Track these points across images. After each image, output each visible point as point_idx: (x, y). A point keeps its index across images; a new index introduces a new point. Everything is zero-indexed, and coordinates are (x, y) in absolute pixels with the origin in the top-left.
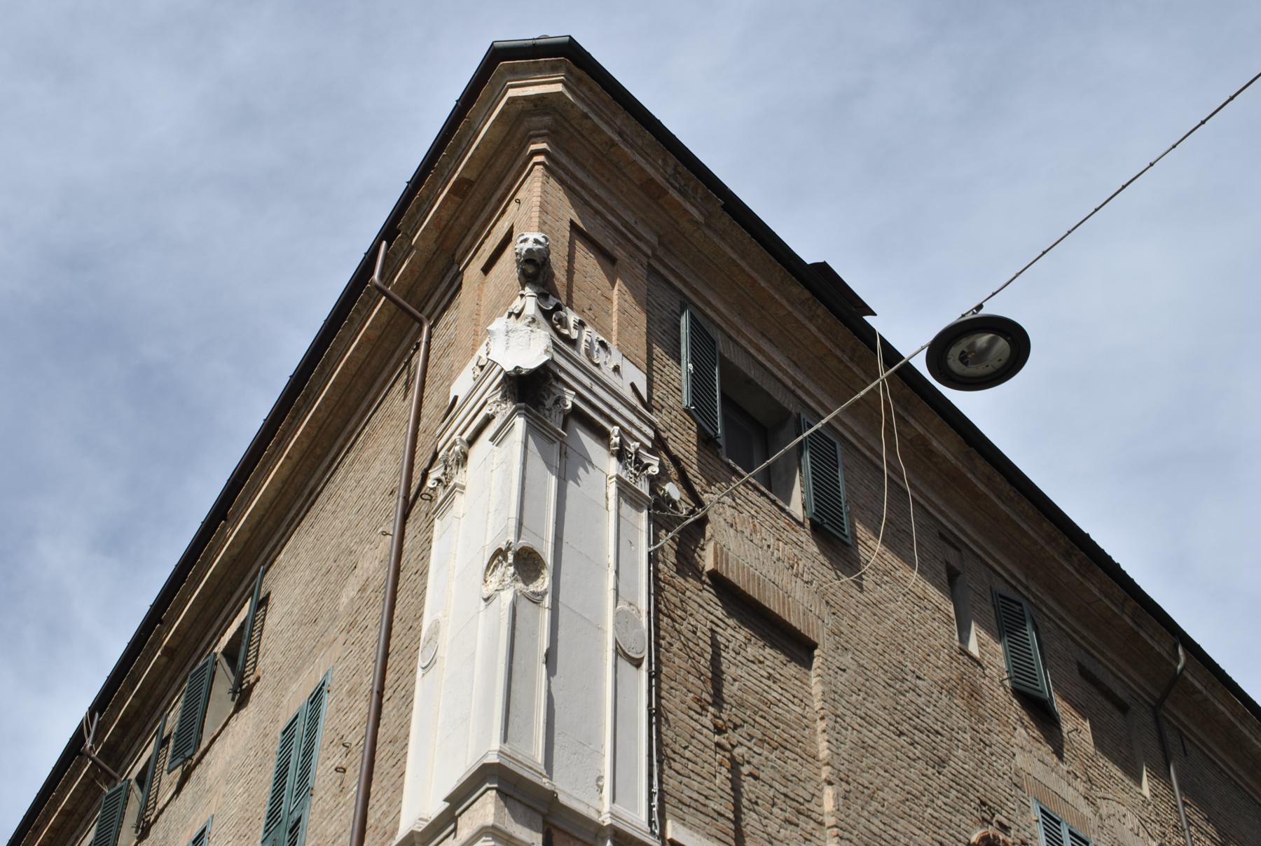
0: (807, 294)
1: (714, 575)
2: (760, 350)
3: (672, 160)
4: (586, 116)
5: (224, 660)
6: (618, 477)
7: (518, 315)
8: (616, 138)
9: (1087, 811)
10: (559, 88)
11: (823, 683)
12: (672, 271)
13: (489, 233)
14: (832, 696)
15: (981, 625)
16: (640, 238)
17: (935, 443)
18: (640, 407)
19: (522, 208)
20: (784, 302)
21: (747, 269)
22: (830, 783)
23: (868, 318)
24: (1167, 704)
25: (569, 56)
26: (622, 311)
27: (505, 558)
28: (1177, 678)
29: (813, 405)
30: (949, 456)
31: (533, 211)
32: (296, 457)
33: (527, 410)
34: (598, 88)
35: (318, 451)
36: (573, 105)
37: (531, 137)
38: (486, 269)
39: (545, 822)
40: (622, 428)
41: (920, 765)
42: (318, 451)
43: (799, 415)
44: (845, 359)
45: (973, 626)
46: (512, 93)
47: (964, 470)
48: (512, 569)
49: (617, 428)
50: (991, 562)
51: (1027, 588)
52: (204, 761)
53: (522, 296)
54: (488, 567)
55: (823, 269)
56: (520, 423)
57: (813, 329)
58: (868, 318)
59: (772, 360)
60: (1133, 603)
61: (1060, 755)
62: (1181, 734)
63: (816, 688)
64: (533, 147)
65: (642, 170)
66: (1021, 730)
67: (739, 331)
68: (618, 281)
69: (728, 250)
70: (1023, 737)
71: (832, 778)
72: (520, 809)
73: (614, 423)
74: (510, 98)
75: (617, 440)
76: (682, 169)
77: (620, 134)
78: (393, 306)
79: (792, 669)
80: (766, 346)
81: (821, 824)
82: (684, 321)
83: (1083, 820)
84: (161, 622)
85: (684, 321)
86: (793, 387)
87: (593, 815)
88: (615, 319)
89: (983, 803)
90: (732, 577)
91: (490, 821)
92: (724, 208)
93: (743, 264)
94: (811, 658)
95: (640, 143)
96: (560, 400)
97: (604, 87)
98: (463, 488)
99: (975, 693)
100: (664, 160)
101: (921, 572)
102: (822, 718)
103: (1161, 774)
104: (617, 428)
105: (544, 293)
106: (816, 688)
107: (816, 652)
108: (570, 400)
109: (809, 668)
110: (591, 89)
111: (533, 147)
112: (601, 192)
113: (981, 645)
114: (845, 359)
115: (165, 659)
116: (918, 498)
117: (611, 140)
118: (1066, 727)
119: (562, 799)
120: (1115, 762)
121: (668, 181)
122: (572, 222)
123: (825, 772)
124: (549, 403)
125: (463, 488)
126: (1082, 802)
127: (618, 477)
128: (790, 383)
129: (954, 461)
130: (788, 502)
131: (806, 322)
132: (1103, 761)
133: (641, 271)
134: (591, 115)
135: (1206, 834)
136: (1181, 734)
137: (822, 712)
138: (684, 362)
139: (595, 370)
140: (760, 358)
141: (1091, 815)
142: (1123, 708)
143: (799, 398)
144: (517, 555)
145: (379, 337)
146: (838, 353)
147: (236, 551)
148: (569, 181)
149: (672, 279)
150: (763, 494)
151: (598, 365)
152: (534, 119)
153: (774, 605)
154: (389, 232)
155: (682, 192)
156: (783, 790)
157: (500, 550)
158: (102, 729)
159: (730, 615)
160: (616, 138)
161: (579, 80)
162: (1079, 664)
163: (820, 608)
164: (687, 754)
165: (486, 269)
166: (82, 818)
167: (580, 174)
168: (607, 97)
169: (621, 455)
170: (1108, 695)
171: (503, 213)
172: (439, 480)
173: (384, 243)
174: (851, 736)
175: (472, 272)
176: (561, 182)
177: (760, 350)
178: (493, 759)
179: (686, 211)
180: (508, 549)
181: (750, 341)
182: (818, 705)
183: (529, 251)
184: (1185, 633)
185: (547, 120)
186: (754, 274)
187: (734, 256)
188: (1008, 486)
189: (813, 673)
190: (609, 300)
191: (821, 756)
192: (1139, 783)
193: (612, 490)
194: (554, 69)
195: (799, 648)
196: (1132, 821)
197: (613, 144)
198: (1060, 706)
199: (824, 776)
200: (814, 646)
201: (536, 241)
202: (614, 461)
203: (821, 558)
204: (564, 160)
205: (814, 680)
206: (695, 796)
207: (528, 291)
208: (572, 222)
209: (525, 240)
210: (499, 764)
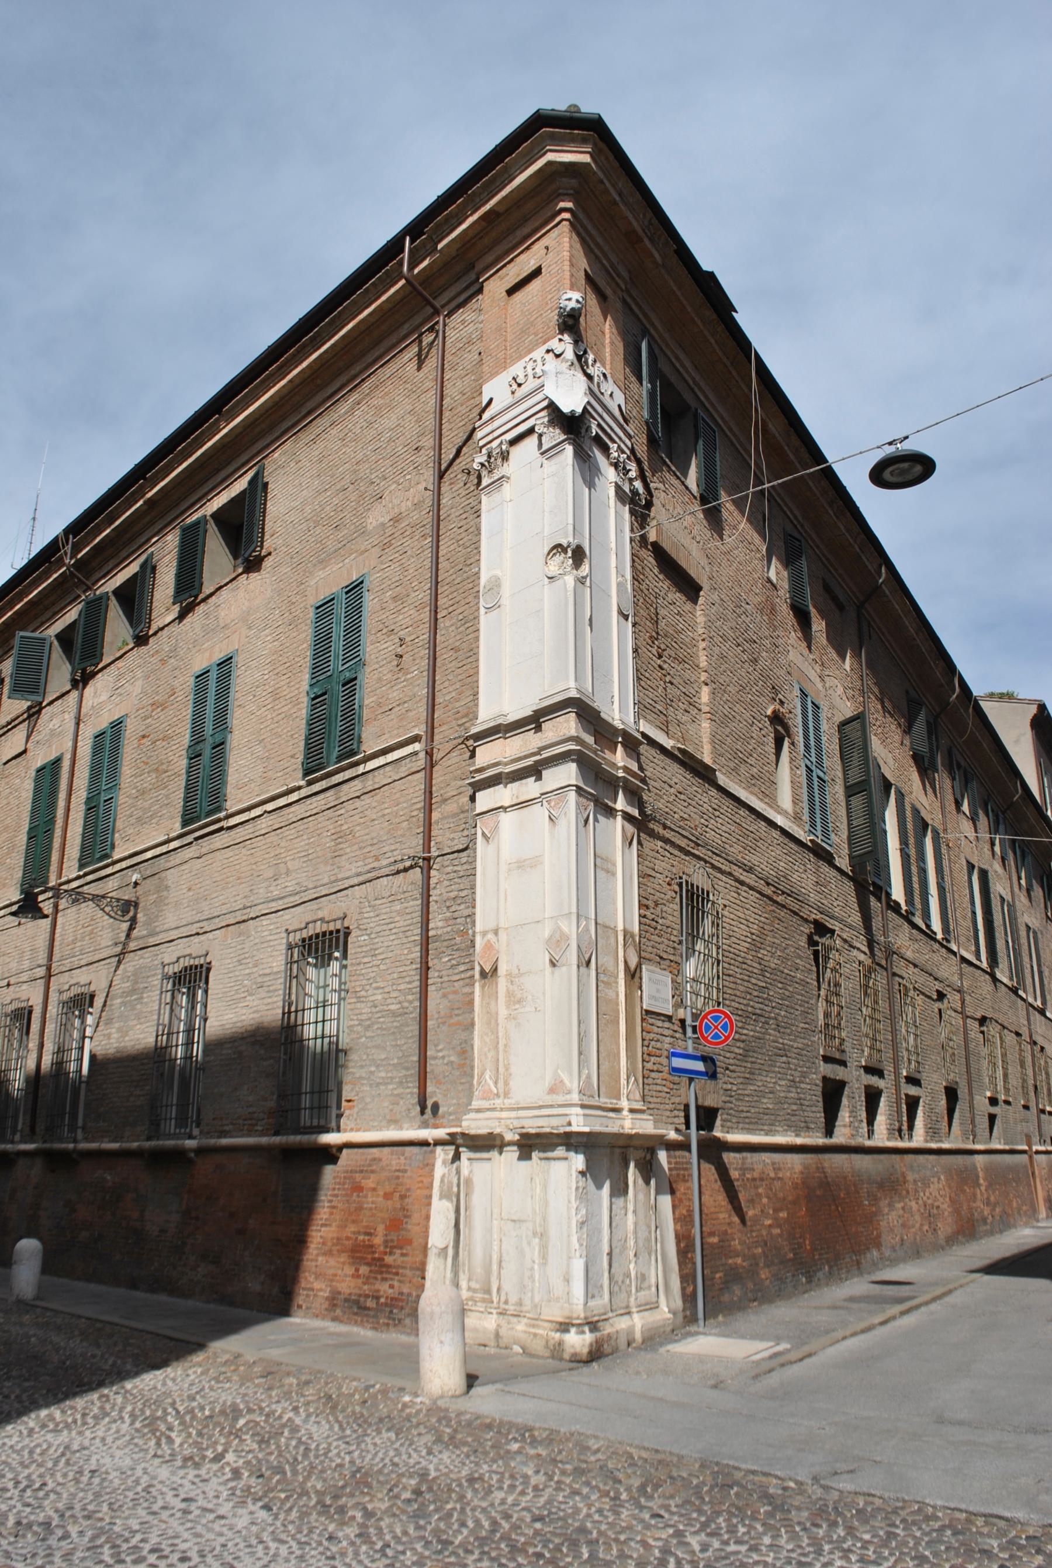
0: (714, 316)
1: (655, 545)
2: (677, 358)
3: (650, 214)
4: (602, 182)
5: (212, 522)
6: (616, 483)
7: (558, 356)
8: (618, 198)
9: (819, 685)
10: (586, 158)
11: (705, 615)
12: (634, 300)
13: (512, 260)
14: (709, 624)
15: (779, 559)
16: (619, 275)
17: (770, 426)
18: (622, 422)
19: (550, 255)
20: (699, 322)
21: (682, 298)
22: (707, 684)
23: (734, 314)
24: (867, 605)
25: (593, 130)
26: (612, 343)
27: (566, 552)
28: (878, 587)
29: (702, 398)
30: (777, 435)
31: (556, 259)
32: (297, 382)
33: (574, 440)
34: (612, 157)
35: (319, 382)
36: (595, 173)
37: (559, 195)
38: (511, 292)
39: (595, 730)
40: (619, 446)
41: (746, 666)
42: (319, 382)
43: (696, 410)
44: (728, 364)
45: (774, 558)
46: (550, 157)
47: (784, 444)
48: (571, 561)
49: (616, 445)
50: (785, 509)
51: (802, 526)
52: (210, 601)
53: (560, 340)
54: (548, 554)
55: (711, 275)
56: (569, 450)
57: (713, 341)
58: (734, 314)
59: (682, 365)
60: (863, 536)
61: (809, 647)
62: (869, 625)
63: (701, 619)
64: (562, 205)
65: (630, 223)
66: (793, 633)
67: (667, 345)
68: (609, 318)
69: (672, 284)
70: (793, 637)
71: (708, 681)
72: (585, 723)
73: (614, 442)
74: (550, 163)
75: (616, 454)
76: (655, 221)
77: (620, 194)
78: (409, 288)
79: (688, 606)
80: (682, 356)
81: (700, 710)
82: (644, 346)
83: (818, 691)
84: (145, 479)
85: (644, 346)
86: (693, 386)
87: (610, 720)
88: (608, 350)
89: (774, 688)
90: (664, 545)
91: (573, 733)
92: (676, 251)
93: (678, 293)
94: (698, 597)
95: (631, 200)
96: (589, 429)
97: (616, 157)
98: (508, 478)
99: (773, 610)
100: (644, 215)
101: (749, 520)
102: (703, 640)
103: (857, 655)
104: (616, 445)
105: (577, 341)
106: (701, 619)
107: (702, 593)
108: (594, 429)
109: (696, 603)
110: (607, 158)
111: (562, 205)
112: (600, 240)
113: (777, 573)
114: (728, 364)
115: (146, 507)
116: (758, 472)
117: (615, 200)
118: (815, 627)
119: (603, 715)
120: (834, 648)
121: (644, 231)
122: (585, 270)
123: (704, 677)
124: (583, 431)
125: (508, 478)
126: (818, 679)
127: (616, 483)
128: (691, 382)
129: (779, 438)
130: (686, 476)
131: (709, 337)
132: (830, 650)
133: (619, 305)
134: (605, 181)
135: (873, 693)
136: (869, 625)
137: (704, 636)
138: (644, 383)
139: (601, 397)
140: (678, 365)
141: (821, 688)
142: (841, 607)
143: (695, 394)
144: (573, 552)
145: (391, 309)
146: (725, 360)
147: (228, 440)
148: (584, 234)
149: (633, 306)
150: (678, 478)
151: (602, 394)
152: (564, 180)
153: (683, 563)
154: (415, 229)
155: (652, 241)
156: (684, 690)
157: (560, 545)
158: (77, 548)
159: (661, 572)
160: (618, 198)
161: (601, 151)
162: (823, 579)
163: (704, 562)
164: (647, 675)
165: (511, 292)
166: (47, 609)
167: (590, 227)
168: (616, 164)
169: (616, 465)
170: (835, 599)
171: (528, 248)
172: (482, 465)
173: (408, 238)
174: (717, 650)
175: (495, 286)
176: (579, 234)
177: (677, 358)
178: (573, 694)
179: (652, 255)
180: (569, 546)
181: (673, 352)
182: (701, 631)
183: (573, 309)
184: (874, 535)
185: (574, 182)
186: (685, 302)
187: (675, 288)
188: (807, 455)
189: (698, 608)
190: (603, 333)
191: (701, 665)
192: (844, 659)
193: (612, 492)
194: (584, 141)
195: (690, 588)
196: (840, 690)
197: (615, 203)
198: (813, 611)
199: (703, 679)
200: (700, 589)
201: (578, 301)
202: (612, 470)
203: (704, 522)
204: (581, 216)
205: (699, 613)
206: (651, 702)
207: (566, 337)
208: (585, 270)
209: (570, 299)
210: (579, 699)
